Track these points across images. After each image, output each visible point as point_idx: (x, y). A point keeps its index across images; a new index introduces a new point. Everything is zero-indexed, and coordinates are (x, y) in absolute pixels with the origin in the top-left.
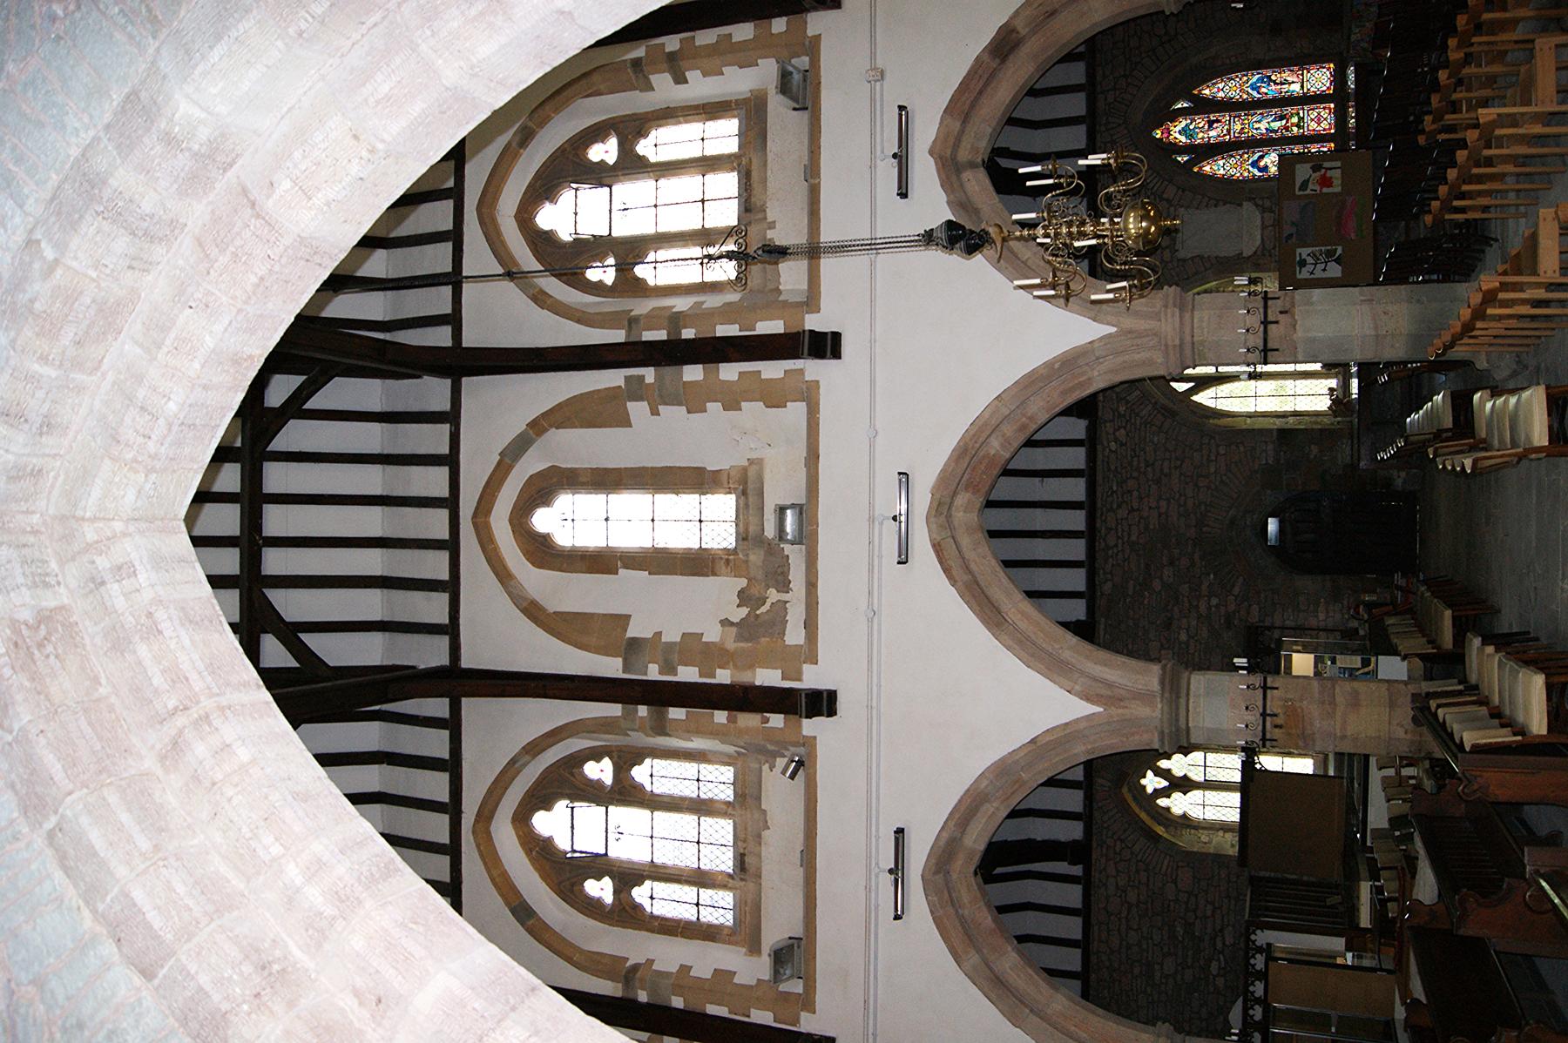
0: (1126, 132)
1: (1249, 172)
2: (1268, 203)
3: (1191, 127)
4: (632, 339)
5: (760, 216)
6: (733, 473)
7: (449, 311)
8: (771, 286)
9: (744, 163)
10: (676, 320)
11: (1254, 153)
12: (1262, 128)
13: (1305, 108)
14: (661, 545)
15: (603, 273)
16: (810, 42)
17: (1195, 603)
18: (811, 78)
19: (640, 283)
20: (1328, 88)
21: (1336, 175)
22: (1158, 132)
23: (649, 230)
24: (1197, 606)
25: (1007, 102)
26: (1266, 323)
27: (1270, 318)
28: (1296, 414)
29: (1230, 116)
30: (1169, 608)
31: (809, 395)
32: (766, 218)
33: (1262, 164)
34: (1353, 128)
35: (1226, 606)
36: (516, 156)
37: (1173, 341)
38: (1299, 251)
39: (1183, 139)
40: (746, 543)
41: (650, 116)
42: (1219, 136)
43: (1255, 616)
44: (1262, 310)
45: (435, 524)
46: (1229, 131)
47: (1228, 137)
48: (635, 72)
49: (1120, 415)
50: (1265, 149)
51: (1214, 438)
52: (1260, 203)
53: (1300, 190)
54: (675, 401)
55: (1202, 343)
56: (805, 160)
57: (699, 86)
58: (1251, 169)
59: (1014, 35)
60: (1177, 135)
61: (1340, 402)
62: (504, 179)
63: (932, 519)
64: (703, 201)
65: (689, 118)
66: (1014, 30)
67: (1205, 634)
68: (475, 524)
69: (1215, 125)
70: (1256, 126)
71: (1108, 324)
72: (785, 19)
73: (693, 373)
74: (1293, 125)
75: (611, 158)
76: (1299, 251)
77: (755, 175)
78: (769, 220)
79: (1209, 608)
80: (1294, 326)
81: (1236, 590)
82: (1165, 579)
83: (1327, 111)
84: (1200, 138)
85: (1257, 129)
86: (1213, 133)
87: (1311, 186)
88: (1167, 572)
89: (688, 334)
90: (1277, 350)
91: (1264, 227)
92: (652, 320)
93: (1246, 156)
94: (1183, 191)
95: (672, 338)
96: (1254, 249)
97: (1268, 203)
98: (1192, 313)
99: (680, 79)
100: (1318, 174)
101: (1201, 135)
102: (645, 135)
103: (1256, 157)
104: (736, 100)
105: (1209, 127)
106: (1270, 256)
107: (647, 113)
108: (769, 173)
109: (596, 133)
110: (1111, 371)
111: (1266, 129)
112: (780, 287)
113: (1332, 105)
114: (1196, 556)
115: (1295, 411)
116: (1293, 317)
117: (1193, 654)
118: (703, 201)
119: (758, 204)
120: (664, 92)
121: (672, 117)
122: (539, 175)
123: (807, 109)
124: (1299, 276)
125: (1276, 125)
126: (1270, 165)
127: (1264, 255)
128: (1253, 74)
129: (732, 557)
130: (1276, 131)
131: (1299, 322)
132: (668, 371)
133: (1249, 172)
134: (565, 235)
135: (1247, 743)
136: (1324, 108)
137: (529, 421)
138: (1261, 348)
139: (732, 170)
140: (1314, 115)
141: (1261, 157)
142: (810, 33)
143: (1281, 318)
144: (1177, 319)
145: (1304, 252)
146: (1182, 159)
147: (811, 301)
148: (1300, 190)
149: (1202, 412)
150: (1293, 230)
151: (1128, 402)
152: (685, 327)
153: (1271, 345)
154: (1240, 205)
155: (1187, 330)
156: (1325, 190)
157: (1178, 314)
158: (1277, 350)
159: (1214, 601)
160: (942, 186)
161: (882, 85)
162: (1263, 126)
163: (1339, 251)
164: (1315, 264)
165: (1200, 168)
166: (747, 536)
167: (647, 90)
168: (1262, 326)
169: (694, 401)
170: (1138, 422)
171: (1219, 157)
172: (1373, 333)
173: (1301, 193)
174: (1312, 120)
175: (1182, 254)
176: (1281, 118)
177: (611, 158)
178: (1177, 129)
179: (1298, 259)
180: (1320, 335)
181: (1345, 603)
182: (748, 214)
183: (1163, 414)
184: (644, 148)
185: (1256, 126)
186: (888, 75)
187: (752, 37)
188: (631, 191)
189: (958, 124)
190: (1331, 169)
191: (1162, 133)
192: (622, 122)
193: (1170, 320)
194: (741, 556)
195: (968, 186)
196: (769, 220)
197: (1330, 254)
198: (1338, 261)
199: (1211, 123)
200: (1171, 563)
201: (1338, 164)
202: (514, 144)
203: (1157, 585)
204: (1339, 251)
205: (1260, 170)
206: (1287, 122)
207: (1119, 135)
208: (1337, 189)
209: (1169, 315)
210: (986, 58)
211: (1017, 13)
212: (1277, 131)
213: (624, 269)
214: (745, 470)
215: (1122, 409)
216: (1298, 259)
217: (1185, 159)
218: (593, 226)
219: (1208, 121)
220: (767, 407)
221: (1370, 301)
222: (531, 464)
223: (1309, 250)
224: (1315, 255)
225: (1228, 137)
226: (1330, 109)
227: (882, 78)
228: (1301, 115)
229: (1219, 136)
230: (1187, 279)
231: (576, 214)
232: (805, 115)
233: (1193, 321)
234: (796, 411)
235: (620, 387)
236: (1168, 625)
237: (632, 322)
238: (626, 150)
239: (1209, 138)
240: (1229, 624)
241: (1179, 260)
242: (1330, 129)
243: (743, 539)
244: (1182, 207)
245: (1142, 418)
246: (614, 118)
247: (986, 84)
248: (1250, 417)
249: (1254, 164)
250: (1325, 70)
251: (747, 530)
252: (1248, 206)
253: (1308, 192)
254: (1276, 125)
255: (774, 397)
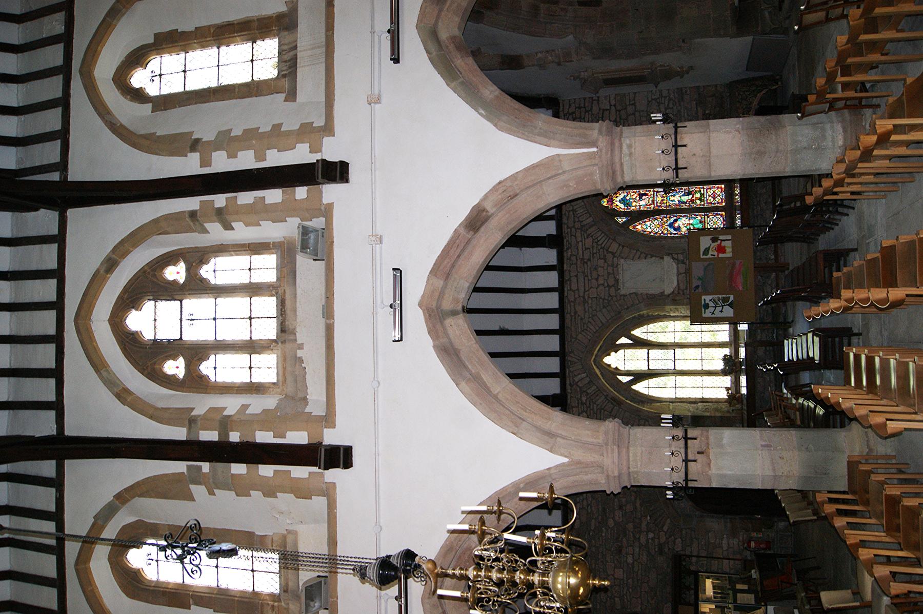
0: (583, 204)
1: (668, 231)
2: (681, 257)
3: (628, 198)
4: (193, 438)
5: (292, 337)
6: (275, 539)
7: (54, 399)
8: (300, 395)
9: (280, 292)
10: (225, 424)
11: (670, 217)
12: (676, 200)
13: (705, 187)
14: (223, 586)
15: (175, 367)
16: (326, 209)
17: (637, 537)
18: (326, 233)
19: (203, 379)
20: (722, 216)
21: (728, 245)
22: (605, 200)
23: (210, 337)
24: (639, 538)
25: (481, 263)
26: (686, 461)
27: (690, 457)
28: (703, 400)
29: (654, 191)
30: (620, 539)
31: (329, 492)
32: (296, 340)
33: (676, 225)
34: (737, 187)
35: (659, 539)
36: (104, 280)
37: (613, 473)
38: (703, 297)
39: (622, 206)
40: (286, 594)
41: (208, 249)
42: (647, 205)
43: (678, 547)
44: (673, 137)
45: (46, 565)
46: (653, 202)
47: (653, 206)
48: (193, 221)
49: (582, 404)
50: (678, 215)
51: (648, 421)
52: (676, 256)
53: (703, 255)
54: (226, 487)
55: (637, 472)
56: (323, 302)
57: (242, 232)
58: (669, 228)
59: (485, 213)
60: (618, 203)
61: (734, 396)
62: (96, 297)
63: (427, 601)
64: (250, 318)
65: (238, 252)
66: (484, 210)
67: (644, 558)
68: (77, 571)
69: (644, 197)
70: (672, 198)
71: (561, 455)
72: (305, 188)
73: (239, 469)
74: (697, 198)
75: (181, 279)
76: (703, 297)
77: (288, 304)
78: (299, 342)
79: (647, 540)
80: (709, 465)
81: (665, 528)
82: (617, 518)
83: (720, 190)
84: (634, 206)
85: (672, 201)
86: (642, 203)
87: (711, 252)
88: (618, 514)
89: (234, 437)
90: (696, 481)
91: (679, 274)
92: (206, 422)
93: (665, 219)
94: (623, 247)
95: (223, 439)
96: (672, 290)
97: (681, 257)
98: (628, 448)
99: (228, 227)
100: (716, 244)
101: (634, 204)
102: (207, 262)
103: (672, 220)
104: (273, 242)
105: (640, 198)
106: (683, 294)
107: (207, 247)
108: (298, 305)
109: (170, 259)
110: (566, 488)
111: (679, 201)
112: (308, 397)
113: (723, 186)
114: (638, 505)
115: (703, 398)
116: (708, 456)
117: (637, 572)
118: (250, 318)
119: (290, 327)
120: (215, 233)
121: (226, 251)
122: (126, 290)
123: (324, 260)
124: (704, 315)
125: (685, 198)
126: (682, 226)
127: (679, 293)
128: (670, 217)
129: (276, 604)
130: (683, 203)
131: (713, 462)
132: (220, 466)
133: (668, 231)
134: (148, 335)
135: (673, 483)
136: (718, 188)
137: (114, 494)
138: (674, 167)
139: (272, 295)
140: (711, 192)
141: (676, 221)
142: (325, 201)
143: (700, 458)
144: (616, 454)
145: (707, 298)
146: (621, 220)
147: (329, 419)
148: (703, 255)
149: (639, 398)
150: (699, 283)
151: (588, 394)
152: (233, 431)
153: (680, 165)
154: (662, 258)
155: (625, 463)
156: (721, 255)
157: (616, 450)
158: (696, 481)
159: (651, 535)
160: (429, 333)
161: (381, 248)
162: (676, 199)
163: (732, 298)
164: (715, 307)
165: (634, 227)
166: (287, 589)
167: (203, 233)
168: (674, 148)
169: (241, 488)
170: (595, 408)
171: (647, 220)
172: (772, 474)
173: (705, 257)
174: (710, 196)
175: (623, 292)
176: (688, 194)
177: (181, 279)
178: (618, 199)
179: (703, 303)
180: (730, 472)
181: (741, 538)
182: (283, 334)
183: (612, 403)
184: (206, 271)
185: (672, 198)
186: (385, 240)
187: (281, 201)
188: (196, 305)
189: (442, 282)
190: (724, 240)
191: (608, 202)
192: (188, 252)
193: (610, 455)
194: (283, 604)
195: (450, 331)
196: (299, 342)
197: (725, 300)
198: (731, 305)
199: (641, 196)
200: (621, 507)
201: (729, 237)
202: (102, 272)
203: (611, 523)
204: (732, 298)
205: (675, 229)
206: (693, 197)
207: (578, 206)
208: (729, 254)
209: (610, 451)
210: (462, 231)
211: (486, 197)
212: (686, 203)
213: (192, 367)
214: (284, 537)
215: (584, 399)
216: (703, 303)
217: (624, 220)
218: (167, 332)
219: (639, 194)
220: (297, 497)
221: (768, 446)
222: (123, 518)
223: (711, 297)
224: (715, 301)
225: (653, 206)
226: (721, 188)
227: (381, 242)
228: (702, 192)
229: (647, 205)
230: (627, 309)
231: (155, 320)
232: (321, 265)
233: (629, 456)
234: (319, 503)
235: (184, 473)
236: (620, 551)
237: (192, 422)
238: (192, 272)
239: (640, 206)
240: (661, 552)
241: (621, 296)
242: (722, 202)
243: (284, 591)
244: (622, 258)
245: (598, 405)
246: (181, 249)
247: (463, 250)
248: (672, 402)
249: (671, 225)
250: (719, 216)
251: (287, 585)
252: (667, 259)
253: (709, 256)
254: (685, 198)
255: (302, 491)
